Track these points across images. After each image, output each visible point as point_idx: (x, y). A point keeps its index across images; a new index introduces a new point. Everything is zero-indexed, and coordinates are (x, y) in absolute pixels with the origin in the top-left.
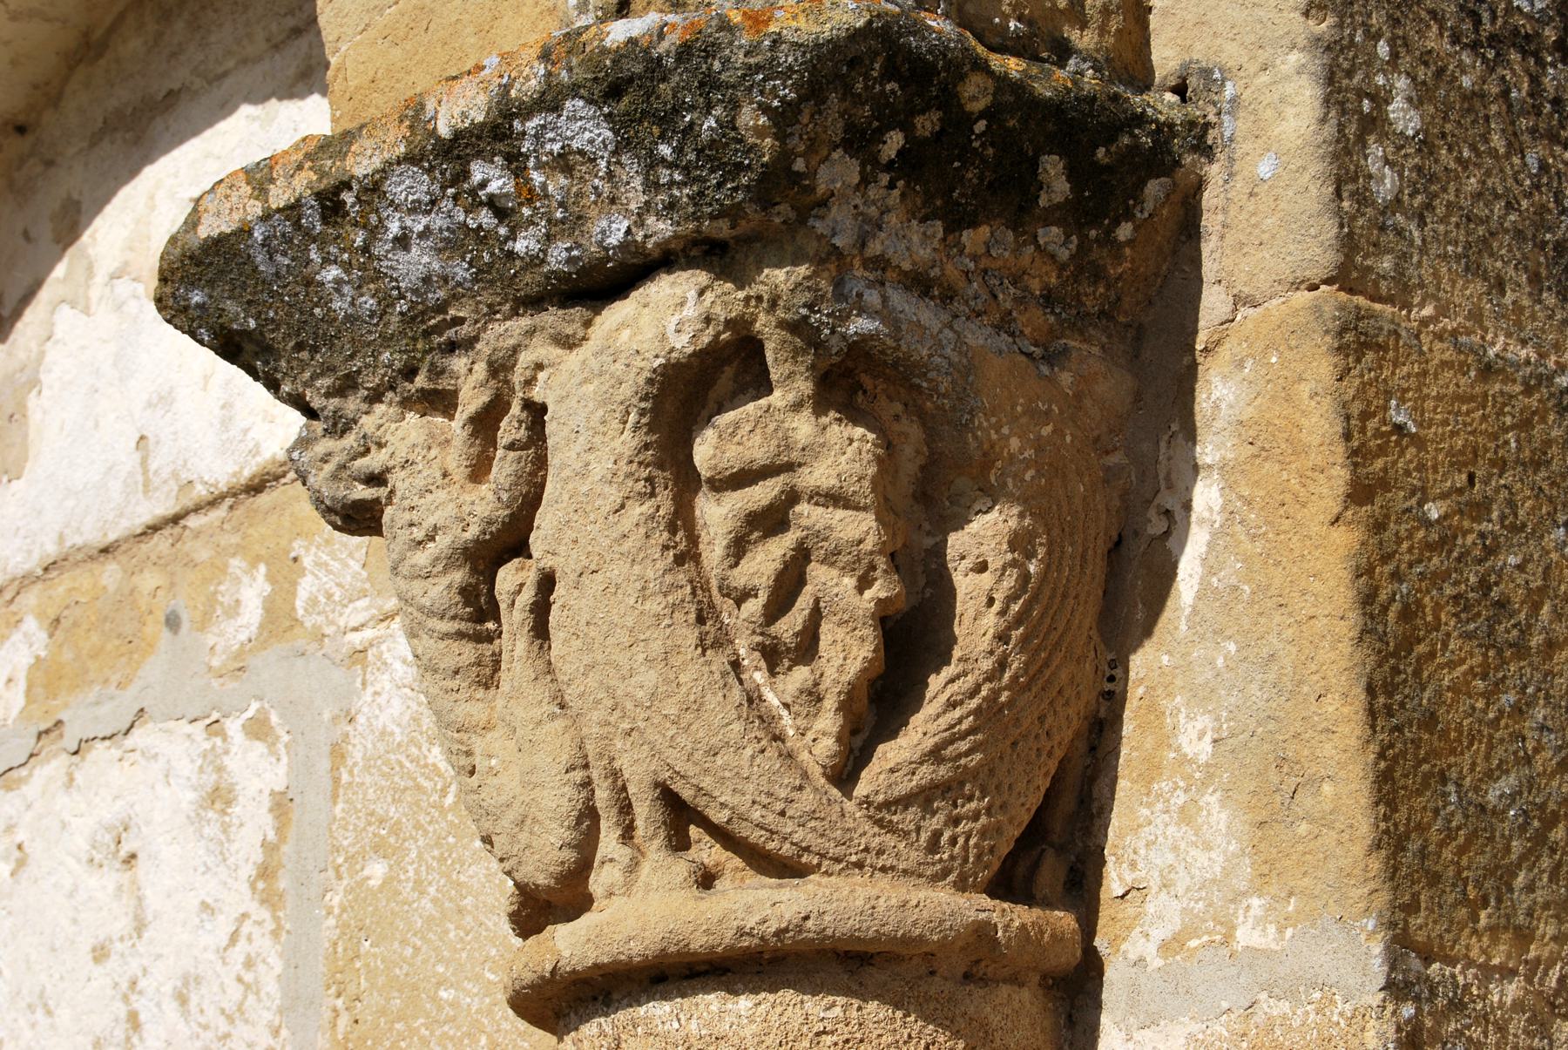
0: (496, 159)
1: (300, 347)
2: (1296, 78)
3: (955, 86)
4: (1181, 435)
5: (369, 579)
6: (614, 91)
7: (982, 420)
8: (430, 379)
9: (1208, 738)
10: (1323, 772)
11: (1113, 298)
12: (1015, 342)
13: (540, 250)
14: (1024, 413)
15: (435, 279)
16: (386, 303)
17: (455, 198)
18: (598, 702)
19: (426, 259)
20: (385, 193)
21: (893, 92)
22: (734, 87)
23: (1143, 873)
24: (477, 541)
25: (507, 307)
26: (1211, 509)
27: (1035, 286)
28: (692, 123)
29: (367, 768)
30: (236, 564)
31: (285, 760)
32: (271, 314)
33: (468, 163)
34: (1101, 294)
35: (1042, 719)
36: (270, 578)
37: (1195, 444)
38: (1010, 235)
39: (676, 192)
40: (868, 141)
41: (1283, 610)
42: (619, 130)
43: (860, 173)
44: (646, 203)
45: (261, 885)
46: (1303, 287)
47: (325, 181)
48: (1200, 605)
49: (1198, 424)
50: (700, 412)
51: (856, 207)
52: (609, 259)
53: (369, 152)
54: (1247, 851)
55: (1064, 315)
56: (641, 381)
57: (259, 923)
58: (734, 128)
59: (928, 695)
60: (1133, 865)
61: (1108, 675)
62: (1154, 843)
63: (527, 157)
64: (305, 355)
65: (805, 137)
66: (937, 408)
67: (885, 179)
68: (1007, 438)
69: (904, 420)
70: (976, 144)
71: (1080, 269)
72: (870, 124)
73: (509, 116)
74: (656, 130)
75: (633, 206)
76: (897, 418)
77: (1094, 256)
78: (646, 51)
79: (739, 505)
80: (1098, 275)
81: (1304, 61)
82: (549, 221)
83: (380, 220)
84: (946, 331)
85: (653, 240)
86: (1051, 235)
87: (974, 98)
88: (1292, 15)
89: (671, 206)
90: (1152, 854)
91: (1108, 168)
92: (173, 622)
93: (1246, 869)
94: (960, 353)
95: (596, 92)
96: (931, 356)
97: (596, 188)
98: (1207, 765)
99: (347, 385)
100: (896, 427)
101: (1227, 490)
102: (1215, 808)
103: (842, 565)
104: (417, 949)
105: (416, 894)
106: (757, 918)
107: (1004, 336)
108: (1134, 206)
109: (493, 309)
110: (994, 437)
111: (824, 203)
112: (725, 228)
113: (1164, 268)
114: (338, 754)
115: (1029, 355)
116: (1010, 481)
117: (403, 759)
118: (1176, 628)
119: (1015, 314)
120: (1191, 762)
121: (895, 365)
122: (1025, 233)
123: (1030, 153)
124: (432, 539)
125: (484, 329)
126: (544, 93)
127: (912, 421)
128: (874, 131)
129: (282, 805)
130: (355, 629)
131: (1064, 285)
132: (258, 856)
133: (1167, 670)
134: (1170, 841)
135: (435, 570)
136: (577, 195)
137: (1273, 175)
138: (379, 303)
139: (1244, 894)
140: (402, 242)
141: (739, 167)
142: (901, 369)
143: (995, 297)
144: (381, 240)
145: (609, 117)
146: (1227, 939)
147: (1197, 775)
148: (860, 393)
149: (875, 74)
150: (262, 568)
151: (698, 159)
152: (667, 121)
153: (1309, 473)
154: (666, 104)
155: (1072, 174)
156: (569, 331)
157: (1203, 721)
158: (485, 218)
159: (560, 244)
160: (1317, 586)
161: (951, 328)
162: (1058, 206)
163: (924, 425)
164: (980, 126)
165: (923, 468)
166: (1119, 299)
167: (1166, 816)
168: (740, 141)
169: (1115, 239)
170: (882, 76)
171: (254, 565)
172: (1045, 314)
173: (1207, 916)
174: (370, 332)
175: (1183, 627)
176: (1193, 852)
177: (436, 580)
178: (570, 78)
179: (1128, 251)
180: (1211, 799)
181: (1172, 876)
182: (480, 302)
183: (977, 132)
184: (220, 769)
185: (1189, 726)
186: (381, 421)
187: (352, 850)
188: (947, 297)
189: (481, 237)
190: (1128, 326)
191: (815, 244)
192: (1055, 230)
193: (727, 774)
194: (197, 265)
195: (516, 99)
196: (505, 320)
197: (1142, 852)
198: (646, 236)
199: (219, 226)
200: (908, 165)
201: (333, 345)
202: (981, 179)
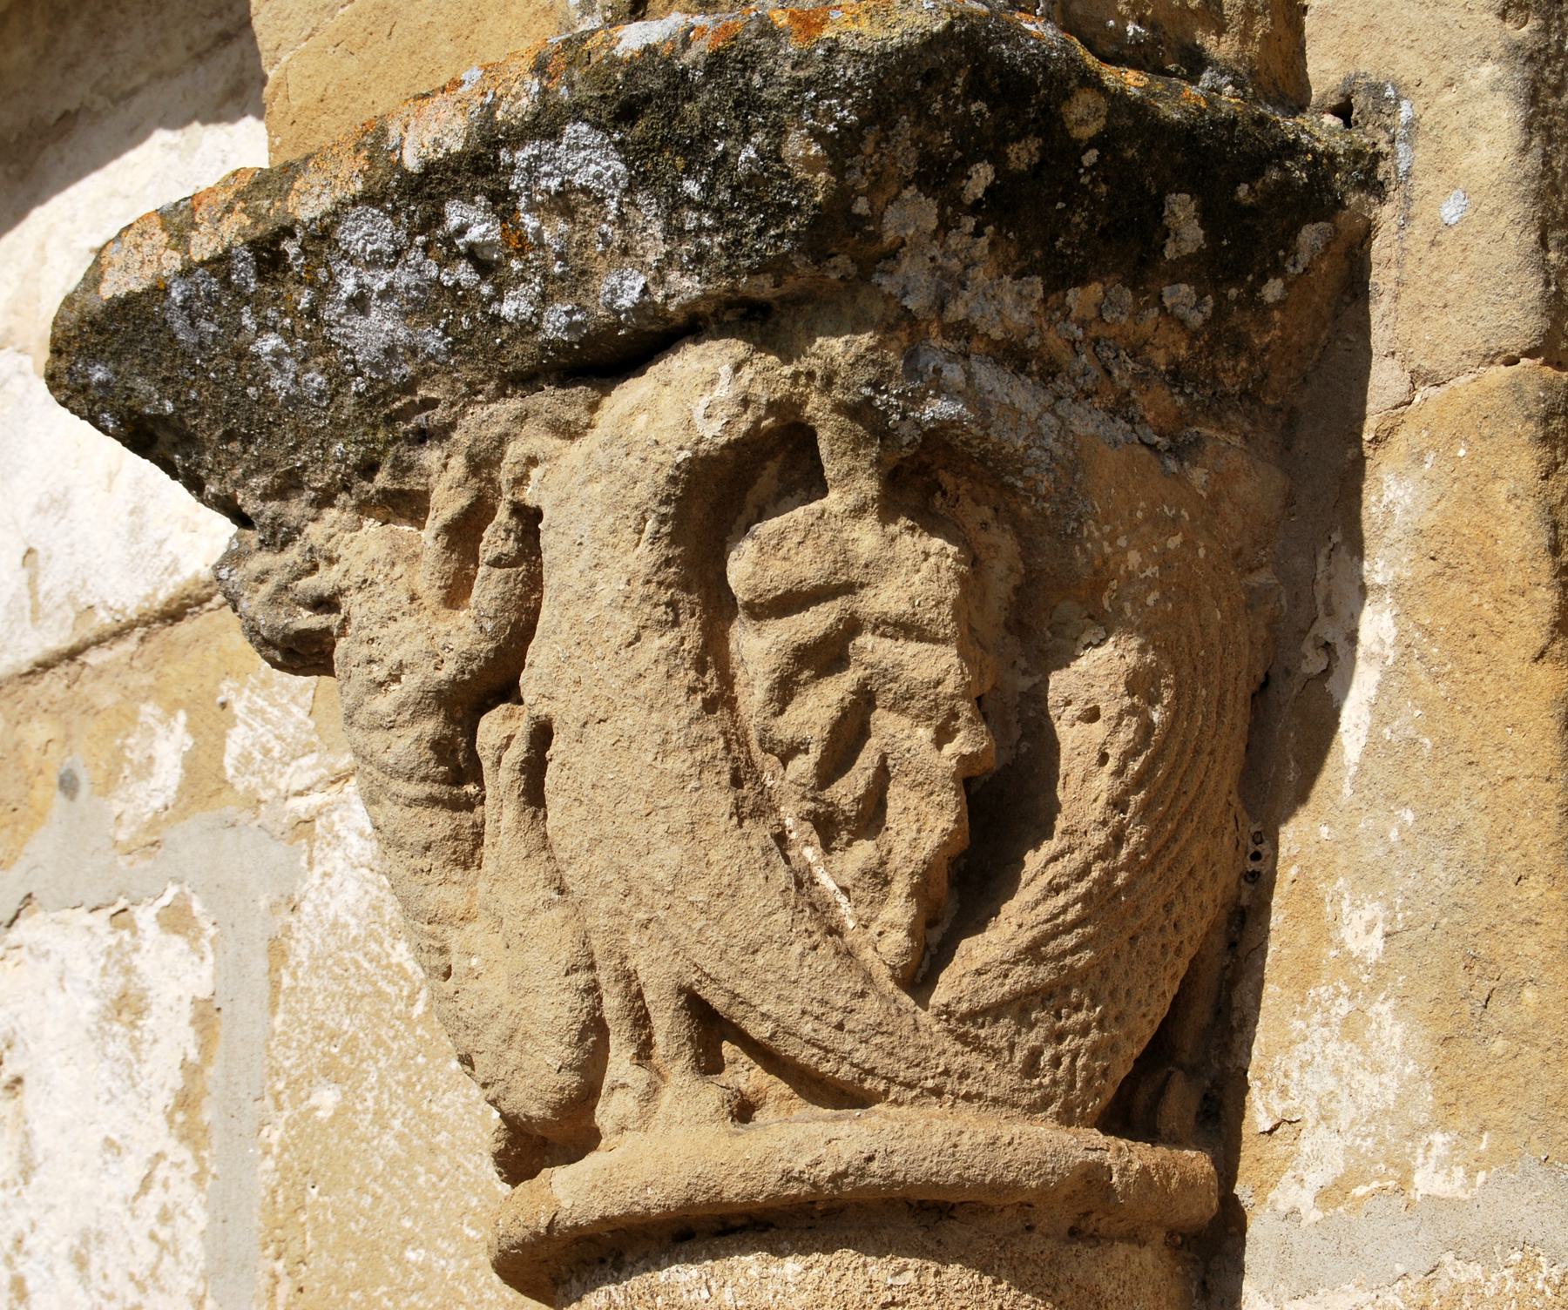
0: (477, 198)
1: (229, 436)
2: (1489, 96)
3: (1058, 106)
4: (1344, 548)
5: (317, 729)
6: (627, 113)
7: (1093, 528)
8: (394, 477)
9: (1378, 932)
10: (1524, 975)
11: (1258, 374)
14: (1146, 520)
16: (338, 379)
17: (426, 248)
18: (606, 885)
19: (388, 325)
21: (980, 113)
22: (778, 107)
23: (1296, 1103)
24: (453, 682)
25: (492, 386)
26: (1382, 642)
27: (1160, 359)
28: (725, 154)
29: (314, 969)
30: (149, 711)
31: (210, 959)
33: (442, 203)
34: (1243, 370)
36: (191, 728)
37: (1361, 559)
38: (1128, 296)
39: (705, 241)
40: (948, 176)
43: (939, 216)
45: (180, 1117)
46: (1498, 360)
47: (261, 227)
49: (1366, 534)
51: (933, 259)
52: (620, 325)
53: (317, 190)
54: (1428, 1074)
55: (1196, 396)
56: (661, 478)
57: (178, 1166)
58: (779, 160)
59: (1025, 877)
61: (1251, 851)
62: (1310, 1064)
63: (517, 197)
64: (235, 446)
66: (1037, 513)
67: (969, 223)
68: (1125, 551)
69: (994, 529)
70: (1085, 180)
71: (1216, 338)
72: (951, 154)
74: (680, 162)
76: (985, 526)
78: (668, 62)
80: (1239, 345)
82: (545, 277)
84: (1048, 417)
85: (676, 301)
86: (1180, 295)
87: (1082, 122)
88: (1485, 16)
89: (699, 258)
91: (1252, 211)
92: (68, 785)
93: (1427, 1096)
94: (1065, 444)
95: (604, 114)
97: (604, 235)
98: (1378, 965)
100: (984, 538)
101: (1403, 618)
102: (1388, 1019)
103: (915, 712)
104: (377, 1198)
105: (376, 1130)
106: (808, 1159)
107: (1120, 423)
108: (1285, 258)
109: (473, 389)
110: (1108, 550)
111: (892, 254)
113: (1323, 336)
114: (277, 951)
115: (1152, 447)
116: (1128, 607)
117: (360, 957)
118: (1338, 792)
119: (1134, 394)
120: (1357, 961)
121: (983, 459)
122: (1146, 292)
123: (1154, 191)
125: (463, 414)
127: (1004, 530)
128: (956, 164)
129: (206, 1016)
130: (299, 794)
131: (1195, 357)
132: (176, 1080)
133: (1327, 846)
135: (400, 719)
136: (579, 244)
137: (1461, 219)
138: (330, 381)
139: (1424, 1129)
140: (359, 303)
141: (785, 209)
142: (990, 464)
143: (1109, 373)
144: (331, 301)
145: (620, 146)
147: (1365, 978)
148: (938, 494)
149: (957, 91)
150: (182, 716)
151: (733, 199)
152: (693, 150)
153: (1506, 596)
155: (1206, 217)
156: (570, 416)
157: (1373, 910)
158: (464, 273)
159: (558, 306)
160: (1517, 739)
161: (1053, 412)
162: (1189, 258)
163: (1019, 535)
164: (1090, 157)
165: (1017, 590)
167: (1325, 1031)
168: (786, 176)
171: (171, 712)
172: (1172, 394)
174: (318, 418)
175: (1347, 791)
176: (1360, 1076)
177: (402, 731)
178: (571, 96)
179: (1277, 315)
180: (1382, 1009)
181: (1333, 1105)
183: (1086, 164)
184: (128, 971)
185: (1355, 916)
186: (332, 531)
187: (295, 1073)
188: (1049, 374)
189: (458, 296)
191: (881, 306)
192: (1184, 288)
193: (770, 977)
197: (1295, 1075)
198: (667, 297)
199: (127, 284)
201: (271, 434)
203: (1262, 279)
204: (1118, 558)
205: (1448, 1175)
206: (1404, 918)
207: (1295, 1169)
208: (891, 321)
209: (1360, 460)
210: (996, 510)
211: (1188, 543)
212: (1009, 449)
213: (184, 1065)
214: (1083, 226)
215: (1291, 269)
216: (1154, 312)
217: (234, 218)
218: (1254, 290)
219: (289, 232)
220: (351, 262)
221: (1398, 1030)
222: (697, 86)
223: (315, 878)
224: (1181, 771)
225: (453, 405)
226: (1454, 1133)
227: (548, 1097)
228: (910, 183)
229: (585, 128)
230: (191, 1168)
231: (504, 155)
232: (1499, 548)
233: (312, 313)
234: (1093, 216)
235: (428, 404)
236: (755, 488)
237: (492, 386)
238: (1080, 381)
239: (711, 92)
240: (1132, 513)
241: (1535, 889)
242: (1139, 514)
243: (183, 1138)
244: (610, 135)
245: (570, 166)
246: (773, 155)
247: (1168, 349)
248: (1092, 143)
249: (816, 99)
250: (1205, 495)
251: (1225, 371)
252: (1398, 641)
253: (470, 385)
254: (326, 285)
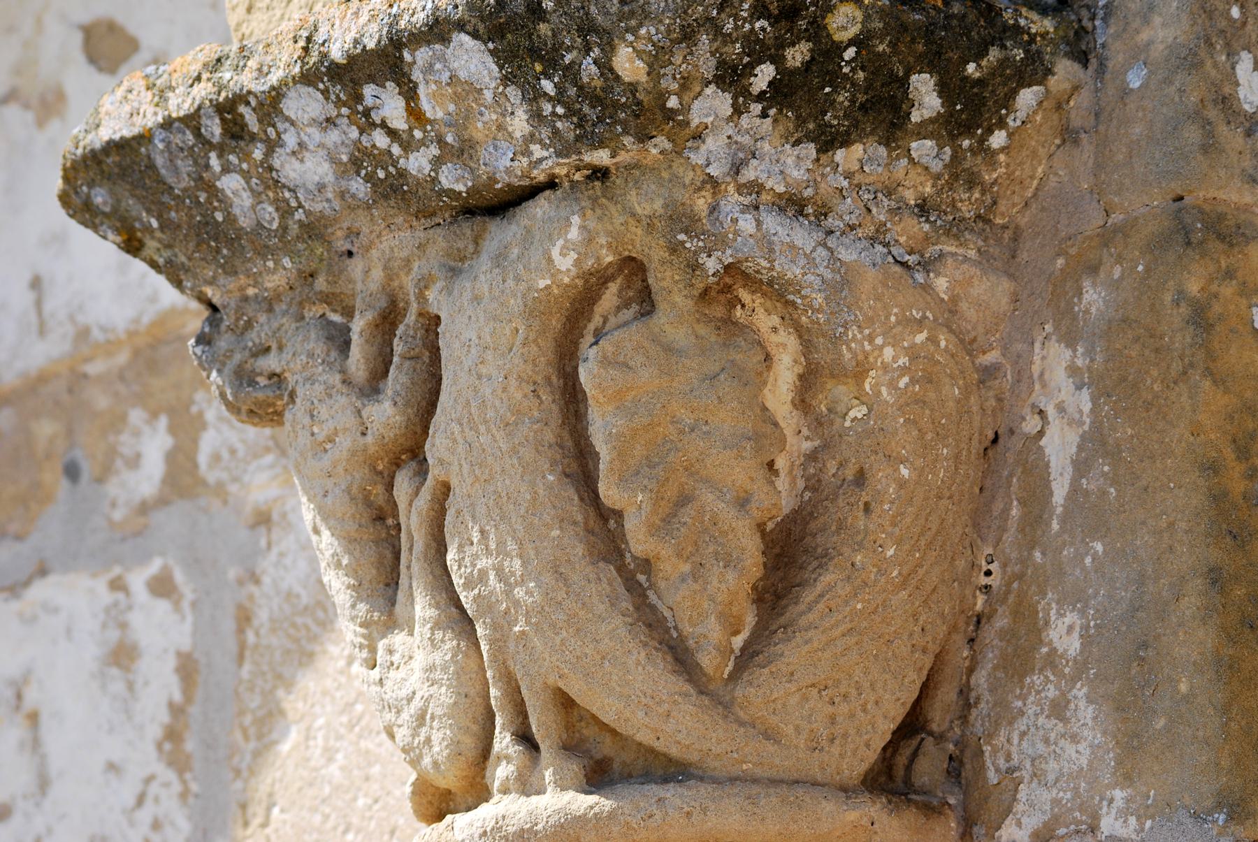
3: (824, 18)
4: (1054, 337)
7: (856, 332)
11: (988, 200)
12: (890, 252)
14: (898, 323)
21: (763, 29)
27: (911, 197)
29: (273, 630)
30: (136, 416)
31: (190, 619)
33: (361, 86)
34: (977, 200)
35: (915, 616)
36: (172, 430)
38: (882, 151)
40: (739, 75)
43: (733, 105)
45: (167, 746)
47: (223, 94)
50: (586, 326)
51: (729, 137)
55: (939, 222)
57: (166, 785)
61: (984, 569)
65: (678, 76)
66: (813, 322)
67: (757, 108)
68: (881, 348)
69: (781, 332)
70: (846, 70)
71: (955, 177)
72: (741, 59)
74: (538, 68)
76: (775, 330)
77: (967, 165)
80: (972, 181)
83: (278, 134)
84: (820, 249)
86: (923, 148)
87: (844, 28)
91: (980, 82)
92: (72, 472)
94: (833, 271)
96: (804, 274)
100: (774, 338)
102: (1082, 704)
107: (879, 248)
108: (1007, 115)
110: (868, 347)
111: (698, 136)
112: (605, 157)
113: (1040, 170)
114: (244, 618)
115: (904, 265)
116: (884, 390)
117: (309, 621)
119: (889, 225)
121: (770, 283)
122: (898, 147)
123: (901, 74)
127: (789, 333)
128: (745, 66)
129: (187, 669)
131: (939, 192)
132: (165, 717)
134: (1041, 732)
142: (776, 286)
143: (869, 210)
146: (1093, 829)
148: (739, 307)
149: (745, 14)
150: (163, 421)
155: (943, 89)
157: (1071, 618)
161: (825, 245)
162: (932, 121)
163: (800, 337)
164: (850, 53)
165: (801, 377)
166: (995, 203)
169: (989, 148)
170: (751, 16)
171: (154, 415)
172: (920, 223)
175: (1055, 526)
179: (1002, 157)
183: (847, 58)
184: (123, 626)
185: (1059, 622)
187: (260, 713)
188: (822, 214)
190: (1005, 227)
191: (691, 174)
192: (928, 143)
199: (120, 129)
200: (778, 94)
202: (853, 101)
203: (990, 131)
204: (876, 353)
205: (1125, 822)
208: (699, 184)
210: (783, 318)
211: (932, 340)
212: (790, 275)
213: (171, 705)
214: (846, 103)
215: (1011, 123)
216: (904, 162)
217: (203, 84)
218: (982, 140)
221: (1091, 708)
223: (273, 556)
224: (924, 514)
228: (710, 83)
230: (177, 787)
231: (407, 56)
234: (854, 96)
236: (601, 302)
238: (847, 218)
240: (887, 318)
242: (893, 319)
243: (170, 764)
244: (485, 44)
247: (915, 188)
248: (851, 42)
250: (946, 298)
251: (961, 201)
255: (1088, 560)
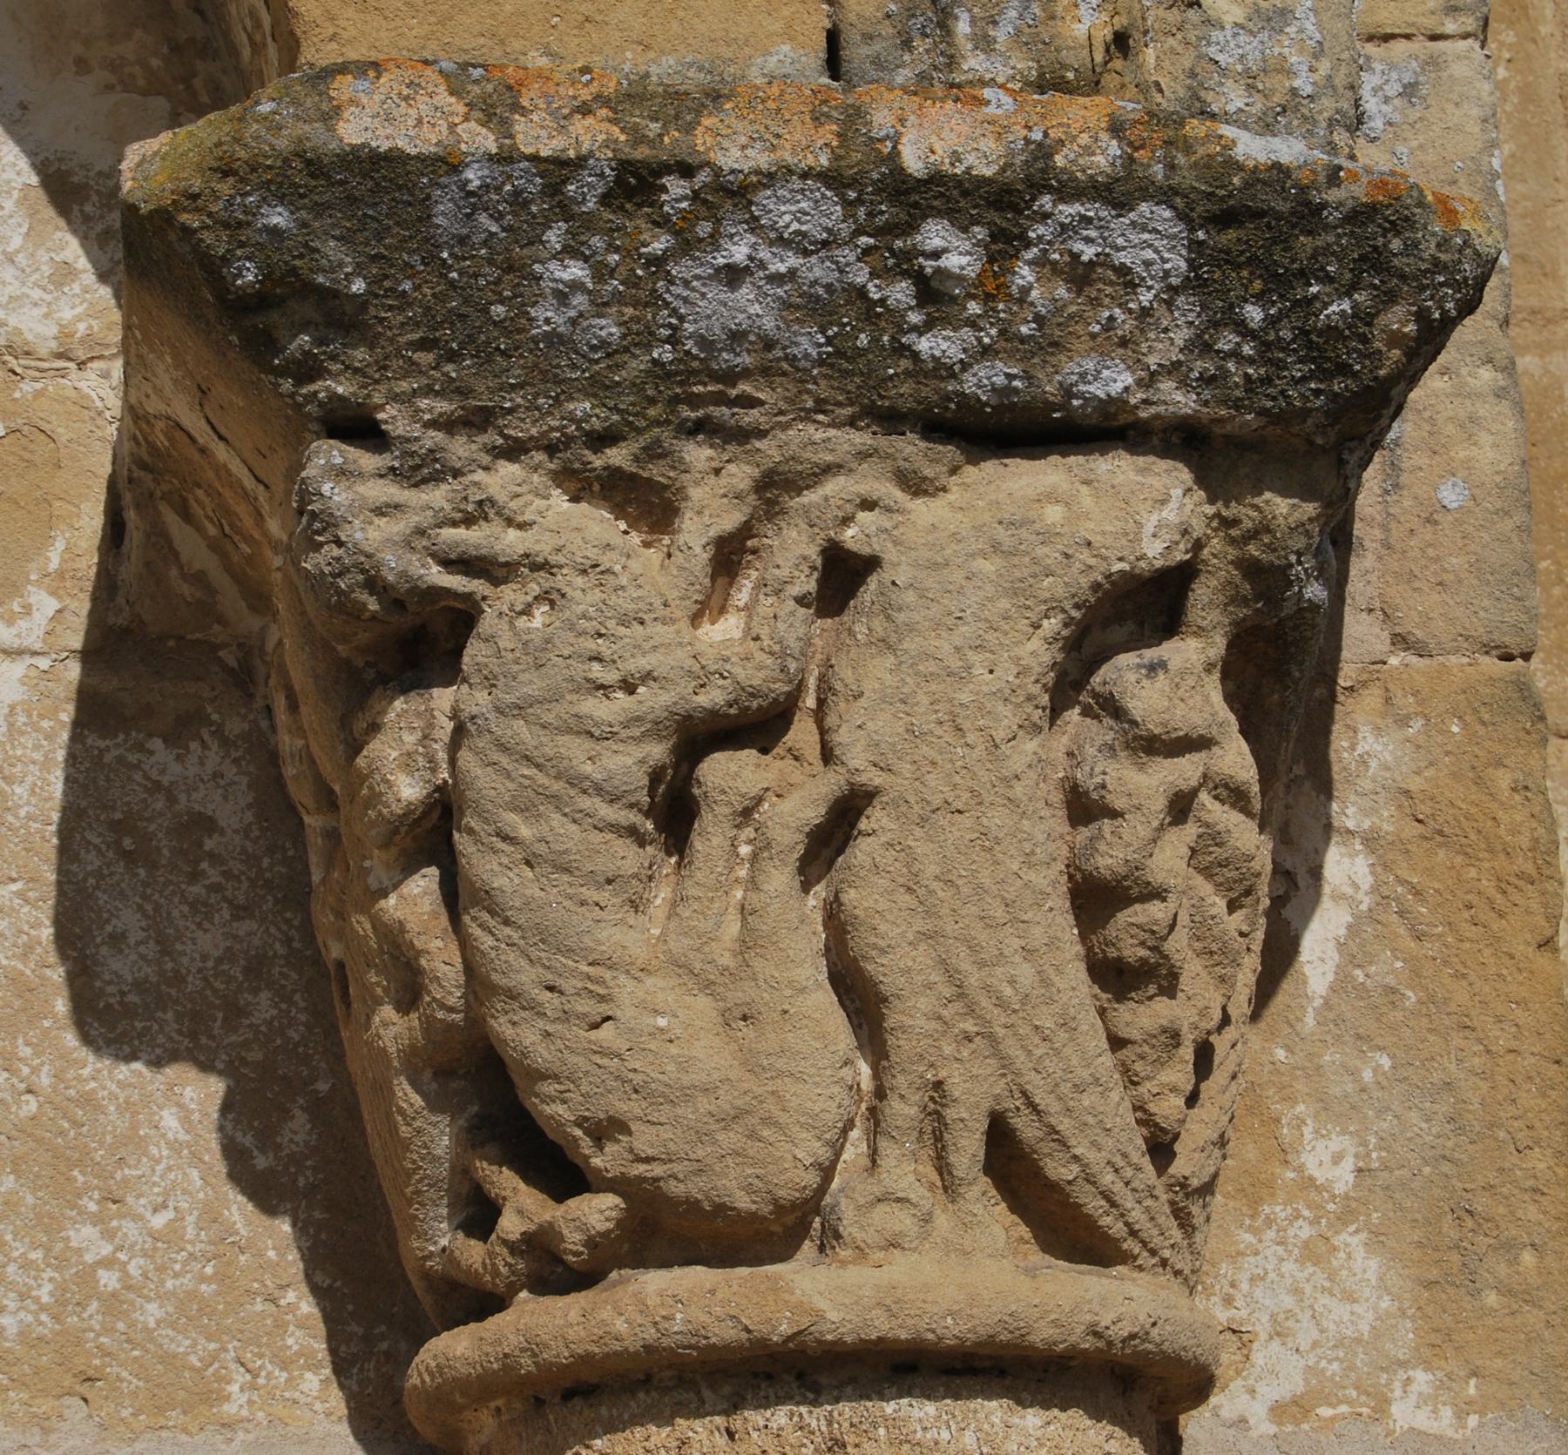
0: (977, 229)
1: (423, 345)
2: (1491, 399)
6: (1225, 219)
8: (636, 459)
9: (1348, 1164)
10: (1526, 1239)
13: (961, 361)
15: (752, 338)
17: (867, 251)
18: (929, 986)
19: (756, 309)
20: (751, 203)
22: (1403, 277)
23: (1244, 1313)
24: (713, 713)
25: (848, 411)
26: (1356, 886)
28: (1316, 297)
32: (407, 286)
33: (924, 217)
39: (1231, 366)
41: (1467, 1033)
42: (1201, 266)
44: (1179, 363)
46: (1494, 652)
48: (1335, 1000)
49: (1335, 777)
52: (1060, 407)
53: (743, 140)
56: (1085, 582)
58: (1370, 324)
59: (1217, 1060)
60: (1228, 1301)
62: (1262, 1279)
63: (1028, 244)
64: (425, 358)
73: (1037, 184)
74: (1258, 285)
75: (1153, 361)
78: (1303, 189)
79: (1171, 778)
81: (1502, 383)
82: (1002, 333)
85: (1153, 410)
88: (1489, 323)
89: (1207, 380)
90: (1258, 1293)
93: (1407, 1333)
95: (1199, 209)
97: (1111, 318)
98: (1347, 1197)
99: (475, 421)
101: (1379, 869)
102: (1360, 1253)
106: (1112, 1316)
109: (821, 406)
118: (1299, 1020)
120: (1319, 1189)
124: (629, 687)
125: (785, 427)
126: (1118, 180)
133: (1282, 1069)
135: (624, 733)
136: (1071, 316)
137: (1461, 507)
138: (624, 337)
139: (1403, 1364)
140: (733, 276)
141: (1344, 370)
144: (694, 259)
145: (1195, 246)
147: (1331, 1207)
151: (1294, 341)
152: (1277, 282)
153: (1513, 880)
154: (1293, 261)
156: (928, 472)
157: (1337, 1143)
158: (901, 293)
159: (999, 364)
160: (1520, 1015)
167: (1280, 1249)
173: (1346, 1382)
174: (574, 367)
175: (1310, 1020)
176: (1325, 1300)
178: (1166, 177)
180: (1351, 1240)
181: (1290, 1323)
182: (808, 392)
186: (518, 489)
189: (870, 311)
193: (1091, 1120)
194: (313, 176)
195: (1063, 170)
196: (829, 425)
197: (1245, 1286)
198: (1145, 401)
201: (489, 361)
206: (1379, 1158)
207: (1245, 1379)
209: (1333, 698)
219: (686, 171)
220: (752, 231)
222: (1327, 225)
225: (781, 413)
226: (1440, 1374)
227: (782, 1193)
229: (1167, 214)
232: (1502, 831)
233: (657, 262)
235: (750, 402)
237: (848, 411)
239: (1339, 236)
241: (1539, 1161)
244: (1192, 230)
245: (1120, 241)
246: (1364, 317)
249: (1442, 284)
252: (1375, 889)
253: (818, 401)
254: (701, 240)
255: (1367, 1075)
